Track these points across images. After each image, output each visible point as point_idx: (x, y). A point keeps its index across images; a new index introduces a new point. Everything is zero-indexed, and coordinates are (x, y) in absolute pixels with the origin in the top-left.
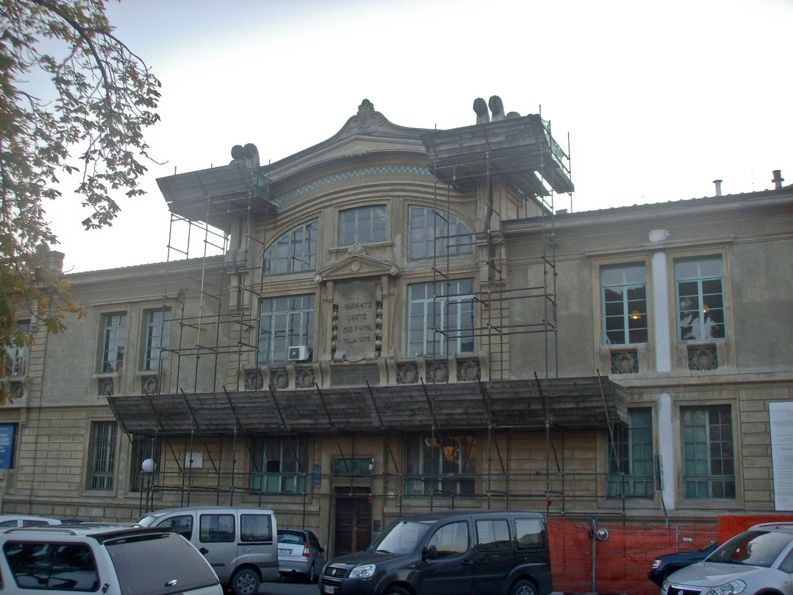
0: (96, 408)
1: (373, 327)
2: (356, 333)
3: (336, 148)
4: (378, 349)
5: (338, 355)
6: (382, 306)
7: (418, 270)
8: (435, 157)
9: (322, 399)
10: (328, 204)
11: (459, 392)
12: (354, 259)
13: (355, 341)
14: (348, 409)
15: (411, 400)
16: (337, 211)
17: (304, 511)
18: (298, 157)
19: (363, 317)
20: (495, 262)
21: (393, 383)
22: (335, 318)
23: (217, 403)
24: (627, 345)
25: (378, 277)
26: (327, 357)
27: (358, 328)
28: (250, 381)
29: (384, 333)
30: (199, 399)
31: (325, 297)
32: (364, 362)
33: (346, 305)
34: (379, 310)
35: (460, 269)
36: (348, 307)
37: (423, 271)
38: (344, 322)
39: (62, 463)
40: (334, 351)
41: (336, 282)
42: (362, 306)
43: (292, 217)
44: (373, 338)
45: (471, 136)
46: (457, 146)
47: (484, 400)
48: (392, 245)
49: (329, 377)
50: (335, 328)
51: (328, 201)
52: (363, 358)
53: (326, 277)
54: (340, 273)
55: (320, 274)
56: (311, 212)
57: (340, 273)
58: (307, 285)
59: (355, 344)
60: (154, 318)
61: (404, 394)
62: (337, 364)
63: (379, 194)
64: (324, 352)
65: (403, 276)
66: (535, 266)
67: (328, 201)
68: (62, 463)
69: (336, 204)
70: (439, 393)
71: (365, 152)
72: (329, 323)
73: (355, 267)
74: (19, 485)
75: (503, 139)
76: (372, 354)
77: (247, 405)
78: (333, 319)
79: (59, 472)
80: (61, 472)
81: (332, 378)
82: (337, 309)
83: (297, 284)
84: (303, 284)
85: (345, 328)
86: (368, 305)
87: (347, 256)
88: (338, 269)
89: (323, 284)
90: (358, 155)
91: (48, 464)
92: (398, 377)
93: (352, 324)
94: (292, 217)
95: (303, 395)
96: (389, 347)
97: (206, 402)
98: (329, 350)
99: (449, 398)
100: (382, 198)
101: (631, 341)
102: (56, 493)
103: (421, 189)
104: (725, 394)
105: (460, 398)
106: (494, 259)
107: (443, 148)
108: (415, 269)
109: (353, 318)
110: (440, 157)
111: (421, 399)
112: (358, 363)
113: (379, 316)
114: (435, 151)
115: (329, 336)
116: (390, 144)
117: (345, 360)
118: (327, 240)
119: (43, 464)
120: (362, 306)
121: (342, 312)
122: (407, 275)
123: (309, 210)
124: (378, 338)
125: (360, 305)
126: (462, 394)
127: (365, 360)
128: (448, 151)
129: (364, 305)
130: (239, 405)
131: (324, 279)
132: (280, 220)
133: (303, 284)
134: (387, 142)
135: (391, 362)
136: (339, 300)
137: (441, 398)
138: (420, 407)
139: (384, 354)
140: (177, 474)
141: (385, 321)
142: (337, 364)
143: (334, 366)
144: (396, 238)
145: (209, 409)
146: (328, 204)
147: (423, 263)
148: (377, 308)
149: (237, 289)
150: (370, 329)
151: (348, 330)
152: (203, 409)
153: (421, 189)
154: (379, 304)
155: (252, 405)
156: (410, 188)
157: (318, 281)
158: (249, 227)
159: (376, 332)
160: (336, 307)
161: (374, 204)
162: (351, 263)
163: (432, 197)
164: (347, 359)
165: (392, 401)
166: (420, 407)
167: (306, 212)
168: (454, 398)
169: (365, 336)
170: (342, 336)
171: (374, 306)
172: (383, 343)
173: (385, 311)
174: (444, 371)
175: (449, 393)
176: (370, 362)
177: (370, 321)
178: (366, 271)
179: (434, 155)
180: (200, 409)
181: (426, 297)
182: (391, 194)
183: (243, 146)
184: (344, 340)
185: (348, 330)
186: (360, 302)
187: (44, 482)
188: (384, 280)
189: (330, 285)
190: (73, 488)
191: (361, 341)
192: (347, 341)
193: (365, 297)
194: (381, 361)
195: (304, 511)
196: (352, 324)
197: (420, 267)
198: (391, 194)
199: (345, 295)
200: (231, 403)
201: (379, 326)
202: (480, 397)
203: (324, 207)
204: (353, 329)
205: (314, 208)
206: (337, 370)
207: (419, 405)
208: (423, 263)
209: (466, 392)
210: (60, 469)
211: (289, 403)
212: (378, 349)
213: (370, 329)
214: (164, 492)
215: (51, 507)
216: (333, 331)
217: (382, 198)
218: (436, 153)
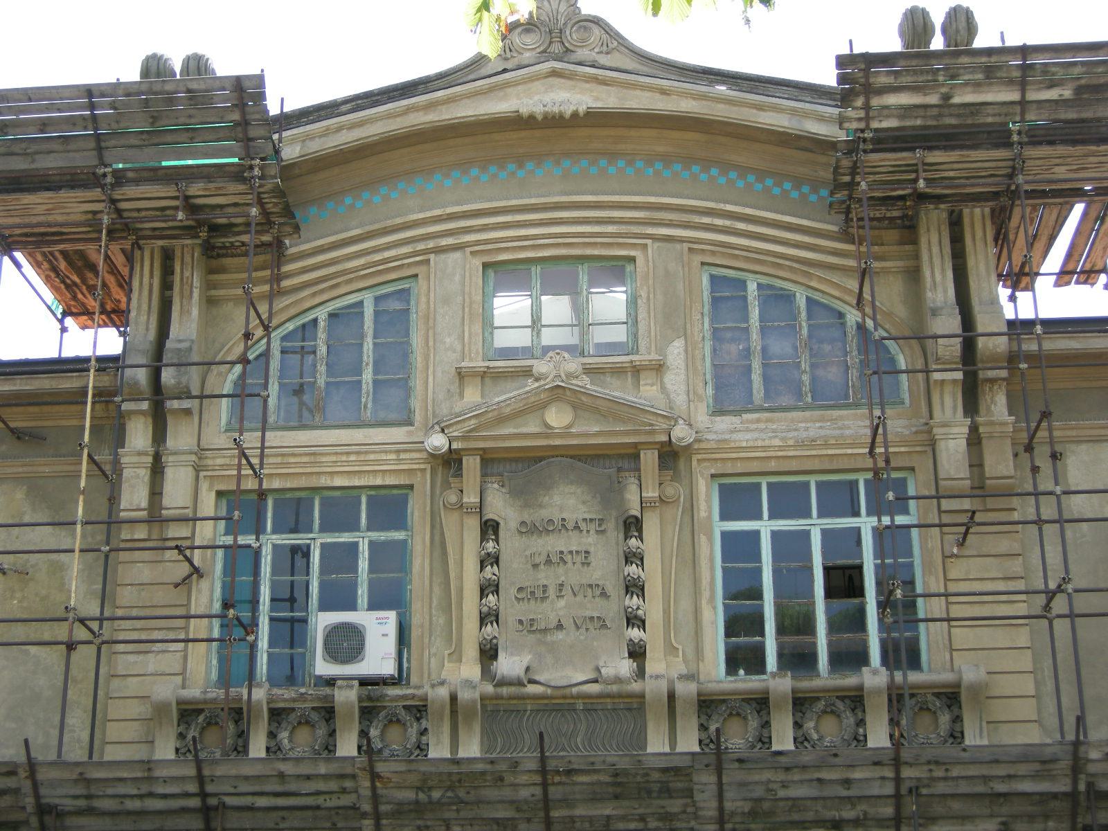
1: (614, 588)
2: (562, 603)
3: (492, 89)
4: (637, 653)
5: (508, 665)
6: (640, 530)
7: (743, 439)
8: (862, 125)
9: (545, 785)
10: (450, 241)
11: (1001, 771)
12: (558, 393)
13: (560, 627)
14: (623, 818)
15: (845, 793)
16: (477, 262)
18: (348, 106)
19: (578, 559)
20: (981, 430)
23: (151, 795)
25: (631, 456)
26: (471, 670)
27: (567, 591)
29: (652, 609)
30: (84, 780)
31: (453, 498)
32: (594, 688)
33: (523, 523)
34: (633, 542)
36: (529, 529)
37: (760, 443)
38: (513, 571)
40: (489, 653)
41: (489, 461)
42: (577, 527)
43: (332, 269)
45: (980, 76)
46: (933, 99)
47: (1073, 796)
48: (659, 368)
49: (477, 728)
50: (488, 588)
51: (450, 233)
52: (591, 676)
53: (464, 438)
54: (508, 430)
55: (443, 431)
56: (395, 259)
57: (508, 430)
58: (386, 462)
59: (560, 635)
60: (971, 262)
61: (825, 775)
62: (505, 691)
63: (610, 229)
64: (457, 656)
65: (698, 451)
66: (1084, 447)
67: (450, 233)
69: (478, 243)
70: (939, 773)
71: (582, 109)
72: (471, 577)
73: (557, 417)
75: (1067, 93)
76: (625, 667)
77: (262, 802)
78: (482, 562)
81: (484, 732)
82: (496, 532)
83: (353, 458)
84: (372, 457)
85: (520, 589)
86: (592, 527)
87: (531, 385)
88: (502, 420)
89: (450, 462)
90: (561, 116)
92: (704, 736)
93: (546, 577)
94: (332, 269)
95: (483, 773)
96: (671, 650)
97: (110, 791)
98: (471, 652)
99: (964, 788)
100: (621, 240)
103: (741, 226)
105: (1001, 788)
106: (980, 420)
107: (892, 100)
108: (734, 436)
109: (549, 562)
110: (875, 125)
111: (876, 791)
112: (575, 690)
113: (634, 557)
114: (867, 107)
115: (471, 605)
116: (657, 96)
117: (532, 681)
118: (448, 340)
120: (577, 527)
121: (510, 544)
122: (713, 450)
123: (387, 254)
124: (635, 620)
125: (570, 525)
126: (1010, 777)
127: (595, 681)
128: (907, 110)
129: (583, 526)
130: (229, 801)
131: (454, 446)
132: (289, 276)
133: (372, 457)
134: (650, 88)
135: (686, 690)
136: (499, 505)
137: (941, 788)
138: (865, 813)
139: (655, 665)
141: (652, 573)
142: (505, 691)
143: (491, 698)
144: (670, 348)
145: (113, 814)
146: (450, 241)
147: (758, 421)
148: (627, 537)
149: (150, 459)
150: (604, 594)
151: (537, 594)
152: (90, 811)
153: (741, 226)
154: (633, 526)
155: (281, 802)
157: (436, 448)
158: (196, 283)
159: (627, 602)
160: (490, 528)
161: (596, 252)
162: (543, 406)
164: (537, 678)
165: (782, 793)
166: (865, 813)
167: (377, 257)
168: (980, 789)
169: (588, 613)
170: (511, 608)
171: (614, 533)
172: (652, 637)
173: (651, 542)
174: (849, 720)
175: (973, 771)
176: (615, 688)
178: (591, 431)
179: (860, 119)
180: (80, 812)
181: (814, 512)
182: (650, 230)
184: (521, 622)
185: (537, 594)
186: (571, 517)
188: (649, 459)
189: (471, 465)
191: (578, 628)
192: (529, 626)
193: (584, 503)
194: (653, 688)
196: (546, 577)
197: (748, 430)
198: (650, 230)
199: (523, 494)
200: (203, 795)
201: (635, 587)
202: (1063, 786)
203: (439, 251)
204: (552, 592)
205: (362, 261)
207: (862, 807)
208: (758, 421)
209: (1022, 769)
211: (422, 796)
212: (637, 653)
213: (604, 594)
217: (621, 240)
218: (867, 114)
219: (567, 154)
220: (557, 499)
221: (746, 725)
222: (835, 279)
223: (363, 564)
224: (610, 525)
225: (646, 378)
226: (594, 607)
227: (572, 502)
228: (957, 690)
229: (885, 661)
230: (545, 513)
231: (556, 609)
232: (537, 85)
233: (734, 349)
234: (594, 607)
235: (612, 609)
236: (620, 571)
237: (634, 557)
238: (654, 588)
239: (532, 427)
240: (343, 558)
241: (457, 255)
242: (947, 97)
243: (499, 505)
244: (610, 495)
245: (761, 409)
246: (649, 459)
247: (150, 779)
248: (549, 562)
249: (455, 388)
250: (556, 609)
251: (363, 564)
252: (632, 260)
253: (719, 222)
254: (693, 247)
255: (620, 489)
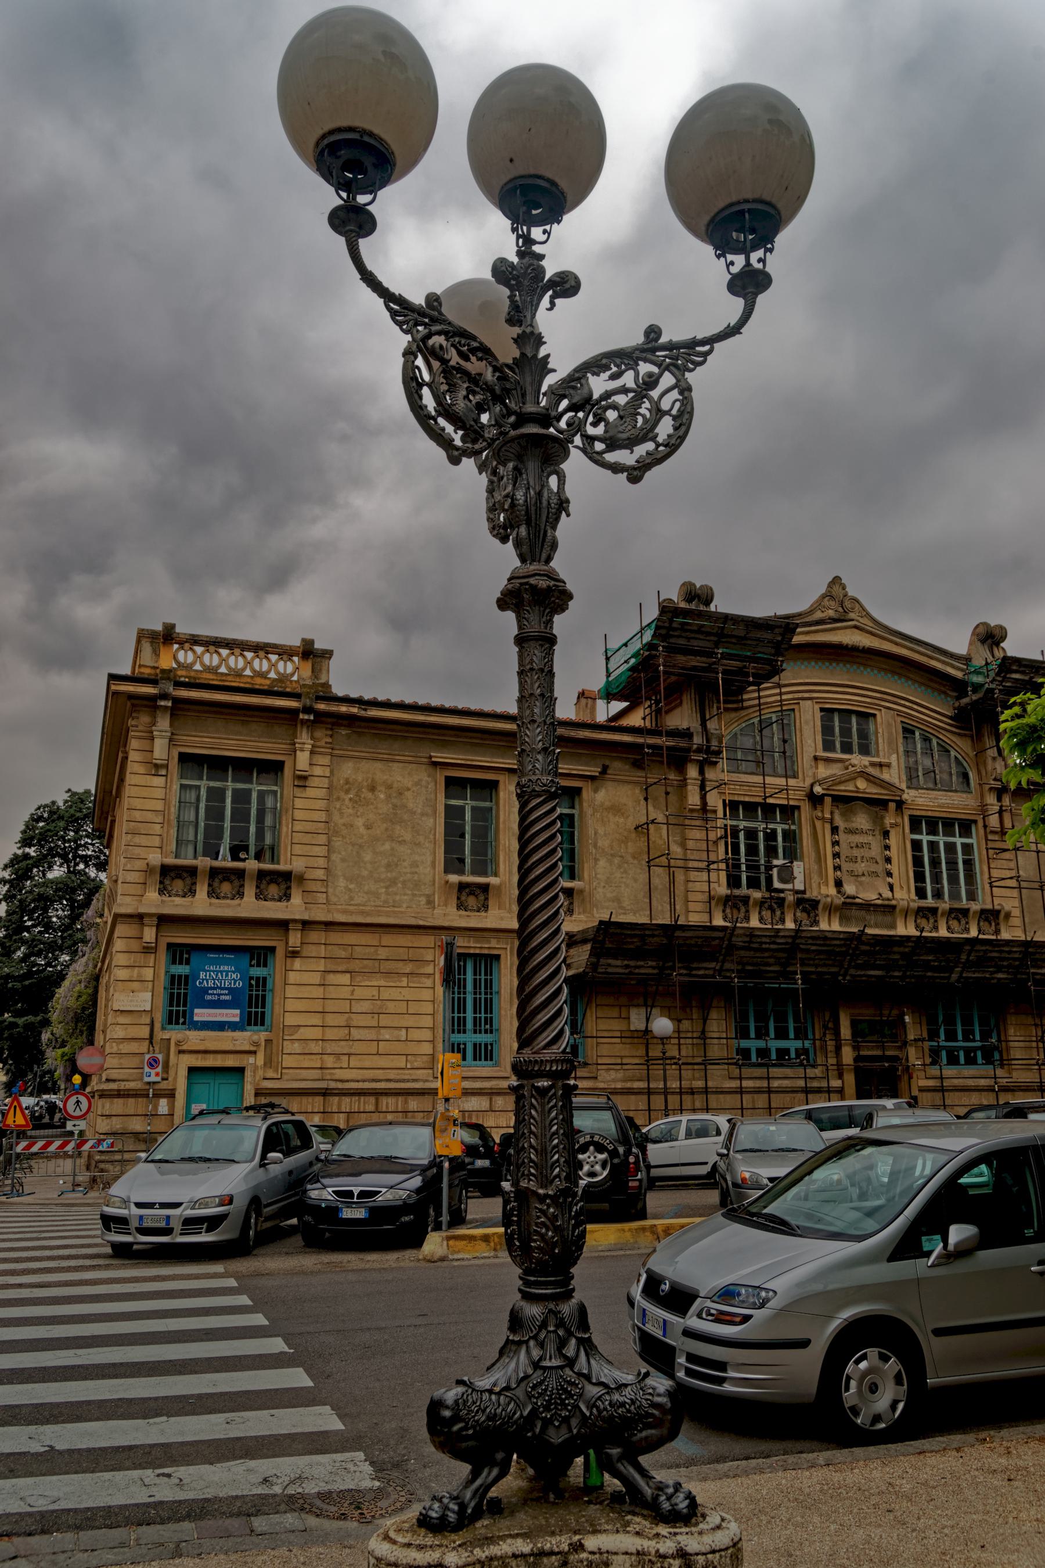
0: (486, 934)
2: (863, 865)
4: (891, 887)
7: (920, 801)
13: (863, 875)
16: (817, 707)
17: (649, 1088)
21: (912, 931)
22: (836, 843)
24: (744, 891)
26: (832, 891)
28: (728, 911)
32: (879, 902)
35: (964, 809)
36: (851, 831)
38: (844, 850)
39: (384, 1020)
40: (839, 884)
44: (882, 874)
50: (836, 855)
57: (843, 788)
59: (863, 878)
63: (868, 700)
68: (384, 1020)
74: (288, 1061)
79: (381, 1038)
80: (387, 1037)
88: (840, 783)
91: (354, 1023)
93: (856, 852)
98: (832, 883)
101: (748, 888)
102: (380, 1074)
103: (915, 707)
104: (494, 943)
109: (857, 846)
119: (343, 1024)
121: (842, 837)
139: (898, 894)
140: (618, 1040)
151: (853, 860)
154: (886, 834)
156: (903, 702)
160: (835, 830)
162: (855, 779)
163: (778, 698)
170: (845, 866)
177: (876, 850)
178: (874, 791)
183: (698, 586)
185: (853, 860)
187: (349, 1055)
188: (892, 806)
189: (828, 800)
190: (416, 1065)
195: (649, 1088)
196: (856, 852)
201: (888, 860)
204: (859, 859)
206: (848, 907)
210: (383, 1031)
212: (891, 887)
214: (599, 1067)
215: (372, 1099)
216: (834, 858)
219: (848, 662)
220: (859, 820)
221: (960, 922)
222: (948, 734)
223: (780, 838)
224: (877, 832)
225: (885, 769)
226: (873, 868)
227: (864, 821)
228: (220, 857)
229: (933, 896)
230: (854, 825)
231: (861, 867)
232: (848, 631)
233: (912, 760)
234: (873, 868)
235: (880, 868)
236: (882, 853)
237: (887, 847)
238: (895, 861)
239: (851, 788)
240: (771, 836)
241: (809, 702)
242: (1032, 678)
243: (839, 821)
244: (878, 820)
245: (923, 788)
246: (892, 806)
247: (776, 936)
248: (857, 846)
249: (813, 763)
250: (861, 867)
251: (780, 838)
252: (874, 715)
253: (907, 704)
254: (899, 714)
255: (882, 818)
